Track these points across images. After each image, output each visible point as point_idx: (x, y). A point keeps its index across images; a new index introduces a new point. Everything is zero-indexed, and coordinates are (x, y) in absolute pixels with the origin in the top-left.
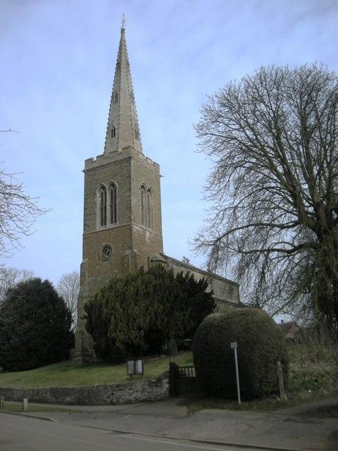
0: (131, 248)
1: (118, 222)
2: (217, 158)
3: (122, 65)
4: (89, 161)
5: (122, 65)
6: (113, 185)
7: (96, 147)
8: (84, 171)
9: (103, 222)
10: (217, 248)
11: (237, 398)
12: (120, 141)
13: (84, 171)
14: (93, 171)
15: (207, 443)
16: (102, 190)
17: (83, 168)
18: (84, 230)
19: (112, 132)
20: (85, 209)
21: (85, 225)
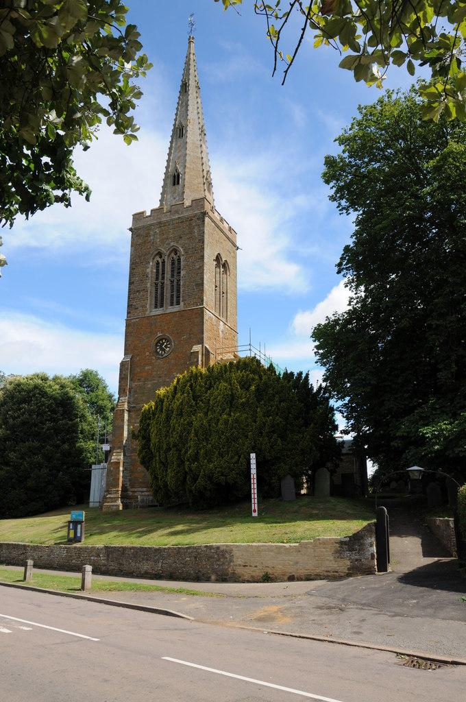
0: (201, 342)
1: (182, 304)
2: (354, 215)
3: (187, 64)
4: (138, 217)
5: (187, 64)
6: (175, 251)
7: (150, 200)
8: (131, 229)
9: (159, 303)
10: (350, 69)
11: (248, 498)
12: (186, 190)
13: (131, 229)
14: (142, 229)
15: (350, 645)
16: (158, 258)
17: (130, 225)
18: (128, 313)
19: (174, 179)
20: (131, 283)
21: (129, 306)
